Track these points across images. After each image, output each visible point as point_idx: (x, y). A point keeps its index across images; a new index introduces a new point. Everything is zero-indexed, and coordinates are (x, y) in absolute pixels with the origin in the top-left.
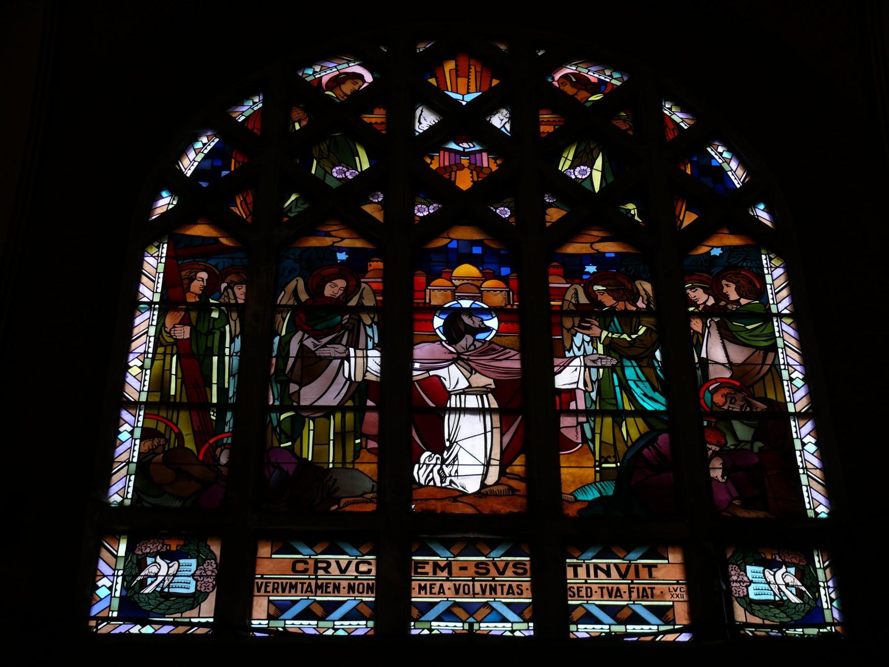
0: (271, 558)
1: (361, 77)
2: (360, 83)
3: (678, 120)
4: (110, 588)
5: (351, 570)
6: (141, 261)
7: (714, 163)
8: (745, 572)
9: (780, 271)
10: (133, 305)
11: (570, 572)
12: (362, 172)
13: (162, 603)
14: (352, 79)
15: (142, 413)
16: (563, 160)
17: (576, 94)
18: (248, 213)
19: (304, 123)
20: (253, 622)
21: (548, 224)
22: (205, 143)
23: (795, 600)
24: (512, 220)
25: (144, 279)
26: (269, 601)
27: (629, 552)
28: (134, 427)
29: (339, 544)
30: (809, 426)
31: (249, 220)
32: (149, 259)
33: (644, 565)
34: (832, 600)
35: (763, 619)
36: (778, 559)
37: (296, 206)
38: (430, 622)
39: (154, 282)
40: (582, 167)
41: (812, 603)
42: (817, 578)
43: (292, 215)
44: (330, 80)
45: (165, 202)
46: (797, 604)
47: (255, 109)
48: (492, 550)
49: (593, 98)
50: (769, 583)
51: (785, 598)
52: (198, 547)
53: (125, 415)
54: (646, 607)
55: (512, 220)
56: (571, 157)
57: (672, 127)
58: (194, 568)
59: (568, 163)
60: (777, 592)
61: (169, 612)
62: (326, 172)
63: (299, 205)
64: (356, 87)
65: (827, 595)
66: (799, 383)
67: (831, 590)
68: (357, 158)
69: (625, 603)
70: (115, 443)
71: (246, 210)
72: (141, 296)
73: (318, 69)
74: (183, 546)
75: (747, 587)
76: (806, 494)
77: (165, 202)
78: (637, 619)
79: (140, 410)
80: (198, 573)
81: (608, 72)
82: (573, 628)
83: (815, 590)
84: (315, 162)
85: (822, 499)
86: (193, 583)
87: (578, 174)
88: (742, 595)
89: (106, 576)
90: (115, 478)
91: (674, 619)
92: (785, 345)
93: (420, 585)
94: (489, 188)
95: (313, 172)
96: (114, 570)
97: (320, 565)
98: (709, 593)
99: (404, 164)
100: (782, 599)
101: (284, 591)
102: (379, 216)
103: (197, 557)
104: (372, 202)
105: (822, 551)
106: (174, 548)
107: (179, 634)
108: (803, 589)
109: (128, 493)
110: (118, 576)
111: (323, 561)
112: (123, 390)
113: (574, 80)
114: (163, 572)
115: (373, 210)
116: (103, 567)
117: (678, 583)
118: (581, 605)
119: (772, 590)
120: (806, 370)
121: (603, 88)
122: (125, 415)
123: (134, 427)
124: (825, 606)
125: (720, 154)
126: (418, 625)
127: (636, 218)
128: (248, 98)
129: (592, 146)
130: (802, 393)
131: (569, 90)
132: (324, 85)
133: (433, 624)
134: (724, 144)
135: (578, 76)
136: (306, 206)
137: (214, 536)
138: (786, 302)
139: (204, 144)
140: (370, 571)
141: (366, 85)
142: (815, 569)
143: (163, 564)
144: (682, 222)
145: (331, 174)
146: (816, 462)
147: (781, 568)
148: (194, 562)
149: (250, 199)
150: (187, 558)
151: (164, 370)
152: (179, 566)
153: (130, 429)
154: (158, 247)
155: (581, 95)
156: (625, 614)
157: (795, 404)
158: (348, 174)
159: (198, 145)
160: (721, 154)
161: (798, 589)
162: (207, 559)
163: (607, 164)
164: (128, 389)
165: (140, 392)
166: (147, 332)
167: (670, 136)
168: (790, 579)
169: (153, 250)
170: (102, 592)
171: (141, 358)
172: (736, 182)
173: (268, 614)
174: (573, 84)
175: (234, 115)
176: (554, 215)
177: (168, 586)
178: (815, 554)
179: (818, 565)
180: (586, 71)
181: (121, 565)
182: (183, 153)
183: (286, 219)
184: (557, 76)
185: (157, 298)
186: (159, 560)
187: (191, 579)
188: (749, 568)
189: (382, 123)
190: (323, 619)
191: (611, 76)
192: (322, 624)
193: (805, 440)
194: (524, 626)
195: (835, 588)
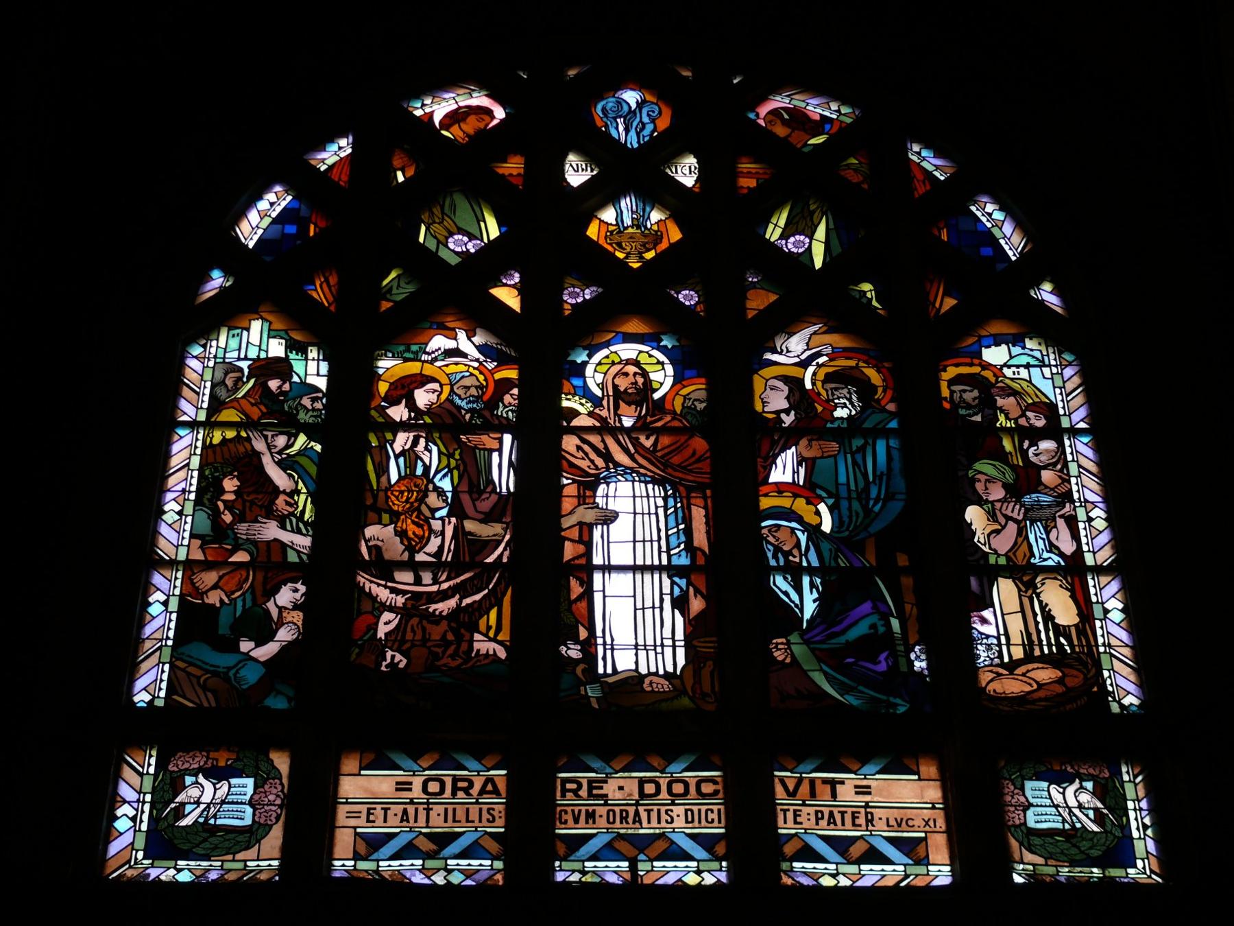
1: (489, 113)
2: (487, 118)
3: (930, 168)
4: (133, 819)
6: (182, 365)
7: (979, 228)
8: (1022, 789)
10: (169, 423)
12: (491, 243)
13: (205, 840)
14: (475, 114)
15: (180, 574)
16: (771, 227)
17: (789, 135)
18: (331, 299)
19: (410, 173)
21: (750, 314)
22: (274, 201)
23: (1095, 828)
25: (186, 392)
26: (356, 834)
27: (863, 764)
28: (168, 596)
30: (1114, 586)
31: (332, 308)
32: (194, 363)
33: (825, 781)
34: (1145, 827)
35: (1046, 859)
36: (1069, 769)
37: (399, 286)
38: (583, 861)
39: (198, 394)
40: (797, 237)
41: (1118, 833)
44: (446, 116)
45: (217, 280)
47: (343, 155)
48: (669, 764)
50: (1056, 807)
51: (1078, 825)
56: (782, 223)
57: (920, 176)
58: (250, 790)
59: (778, 232)
63: (402, 284)
64: (482, 125)
65: (1138, 817)
66: (1100, 524)
67: (1144, 813)
68: (482, 224)
69: (859, 834)
72: (180, 413)
75: (1024, 811)
77: (217, 280)
78: (873, 856)
79: (177, 570)
80: (257, 797)
81: (834, 106)
82: (785, 866)
83: (1121, 813)
84: (423, 228)
86: (249, 810)
87: (793, 245)
88: (1017, 822)
89: (129, 803)
90: (144, 666)
91: (927, 856)
93: (587, 811)
94: (674, 265)
95: (421, 240)
96: (139, 793)
98: (978, 823)
99: (547, 233)
101: (576, 821)
103: (255, 776)
105: (1131, 762)
106: (222, 764)
108: (1105, 811)
110: (144, 802)
111: (463, 779)
112: (154, 543)
113: (786, 116)
114: (206, 798)
116: (125, 791)
117: (933, 808)
118: (861, 837)
119: (1060, 815)
120: (1108, 507)
121: (827, 127)
122: (157, 579)
123: (168, 596)
124: (1135, 834)
125: (989, 212)
126: (565, 865)
127: (875, 303)
128: (332, 141)
129: (812, 207)
130: (1104, 538)
131: (781, 131)
133: (587, 864)
134: (996, 200)
138: (1082, 413)
139: (272, 204)
140: (716, 792)
141: (495, 122)
142: (1122, 783)
146: (1124, 635)
147: (1072, 782)
148: (250, 782)
149: (333, 280)
151: (1029, 635)
152: (230, 787)
153: (163, 598)
154: (204, 346)
156: (857, 850)
157: (1094, 553)
159: (263, 205)
160: (990, 215)
161: (1096, 810)
162: (268, 779)
164: (162, 543)
165: (177, 547)
166: (188, 465)
167: (921, 189)
168: (1085, 798)
170: (122, 824)
171: (181, 500)
172: (1010, 253)
173: (355, 851)
174: (785, 123)
175: (313, 162)
176: (758, 301)
177: (215, 816)
179: (1126, 778)
182: (242, 214)
184: (764, 110)
185: (202, 417)
186: (201, 779)
187: (1032, 800)
188: (1029, 785)
189: (519, 175)
190: (365, 859)
191: (838, 111)
192: (430, 864)
193: (1108, 606)
194: (715, 865)
195: (1151, 811)
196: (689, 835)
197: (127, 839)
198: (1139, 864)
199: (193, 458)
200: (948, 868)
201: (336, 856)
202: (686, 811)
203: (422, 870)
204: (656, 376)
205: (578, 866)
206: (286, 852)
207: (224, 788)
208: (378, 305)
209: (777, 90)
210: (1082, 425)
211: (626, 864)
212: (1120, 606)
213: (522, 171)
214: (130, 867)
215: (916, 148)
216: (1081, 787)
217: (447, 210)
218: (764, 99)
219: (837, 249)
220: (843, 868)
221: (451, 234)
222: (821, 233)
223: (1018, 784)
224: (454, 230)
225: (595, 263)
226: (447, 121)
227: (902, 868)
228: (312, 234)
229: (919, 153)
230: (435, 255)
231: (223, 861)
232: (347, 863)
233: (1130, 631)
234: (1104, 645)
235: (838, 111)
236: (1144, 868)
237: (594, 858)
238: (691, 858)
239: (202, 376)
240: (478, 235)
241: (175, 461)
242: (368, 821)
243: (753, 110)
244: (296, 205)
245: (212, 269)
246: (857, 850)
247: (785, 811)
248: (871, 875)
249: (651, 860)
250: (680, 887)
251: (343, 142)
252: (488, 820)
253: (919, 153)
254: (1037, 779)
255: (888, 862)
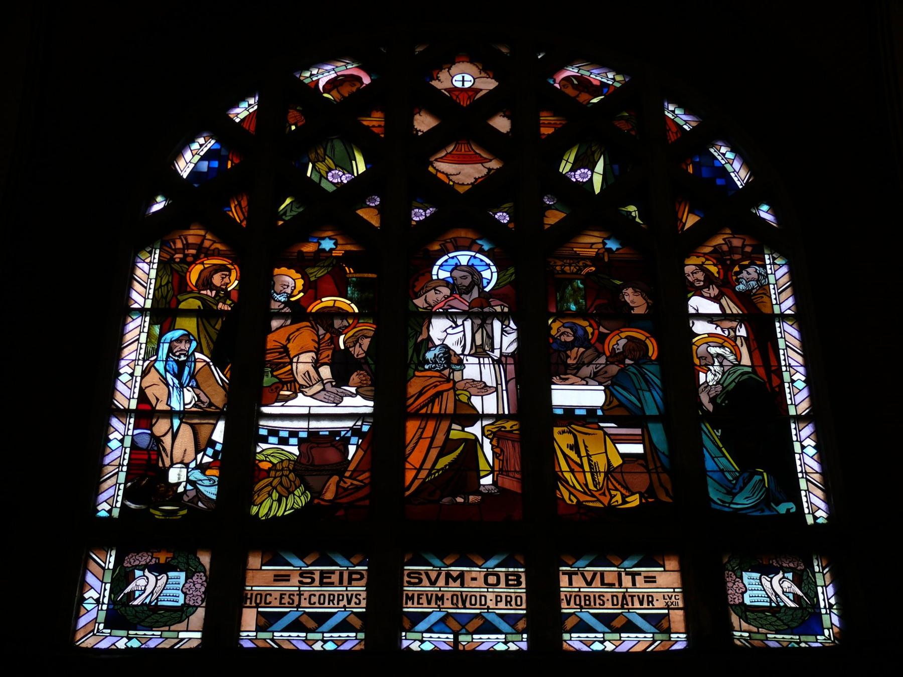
0: (261, 569)
1: (359, 79)
2: (358, 85)
3: (681, 123)
5: (662, 586)
6: (134, 266)
8: (741, 578)
9: (784, 269)
10: (126, 311)
11: (564, 580)
13: (149, 616)
15: (132, 420)
16: (564, 162)
17: (578, 96)
18: (242, 218)
20: (242, 634)
23: (793, 605)
24: (511, 226)
25: (137, 286)
28: (124, 436)
29: (330, 555)
30: (807, 430)
31: (244, 224)
35: (758, 628)
37: (291, 210)
38: (422, 633)
39: (146, 288)
40: (583, 170)
42: (815, 582)
43: (287, 218)
44: (328, 83)
45: (159, 204)
46: (791, 608)
47: (251, 110)
49: (595, 100)
51: (782, 604)
52: (188, 559)
53: (115, 422)
54: (594, 615)
55: (511, 226)
56: (572, 159)
57: (674, 129)
58: (182, 581)
59: (569, 166)
60: (773, 598)
61: (157, 625)
62: (321, 176)
66: (800, 385)
68: (354, 162)
70: (104, 450)
71: (240, 214)
73: (315, 71)
74: (173, 558)
75: (743, 593)
76: (804, 499)
77: (159, 204)
79: (130, 418)
81: (610, 75)
82: (566, 636)
84: (310, 165)
85: (822, 505)
86: (182, 596)
87: (580, 176)
88: (737, 602)
91: (669, 628)
92: (787, 346)
93: (437, 595)
94: (486, 192)
95: (309, 174)
97: (354, 576)
98: (707, 601)
99: (401, 169)
100: (778, 605)
102: (375, 222)
104: (369, 206)
105: (820, 556)
107: (165, 649)
109: (117, 501)
112: (112, 397)
113: (576, 82)
115: (370, 215)
121: (605, 90)
122: (115, 422)
125: (723, 153)
126: (411, 635)
127: (638, 220)
128: (244, 100)
129: (593, 149)
131: (570, 91)
132: (321, 87)
133: (425, 635)
135: (580, 78)
136: (301, 210)
137: (205, 548)
138: (790, 302)
139: (201, 146)
142: (814, 573)
143: (152, 578)
144: (684, 224)
145: (327, 179)
146: (816, 466)
147: (777, 573)
148: (183, 575)
149: (244, 203)
150: (176, 571)
152: (168, 578)
153: (120, 437)
155: (583, 98)
156: (617, 623)
157: (796, 406)
158: (343, 178)
159: (195, 146)
160: (724, 155)
161: (795, 595)
162: (196, 572)
163: (608, 166)
164: (118, 396)
165: (129, 400)
166: (138, 340)
167: (672, 137)
169: (144, 255)
171: (132, 365)
172: (739, 183)
175: (231, 116)
176: (553, 218)
177: (157, 598)
178: (814, 557)
179: (817, 569)
180: (588, 74)
181: (108, 578)
182: (179, 153)
183: (280, 223)
185: (148, 305)
186: (147, 573)
188: (745, 575)
189: (380, 126)
190: (313, 631)
192: (311, 636)
193: (805, 444)
194: (518, 637)
196: (641, 615)
197: (93, 615)
198: (826, 632)
199: (142, 334)
200: (684, 636)
201: (242, 629)
202: (612, 596)
203: (306, 641)
204: (486, 274)
205: (418, 636)
206: (207, 629)
207: (163, 578)
208: (277, 223)
209: (570, 63)
210: (789, 312)
211: (451, 636)
212: (813, 444)
213: (383, 124)
214: (94, 635)
215: (671, 108)
216: (784, 577)
217: (328, 153)
218: (561, 67)
219: (611, 181)
220: (608, 636)
221: (330, 170)
222: (600, 167)
223: (739, 574)
224: (333, 166)
225: (439, 192)
226: (328, 87)
227: (651, 635)
228: (229, 166)
229: (673, 112)
230: (318, 185)
231: (162, 631)
232: (251, 634)
233: (821, 462)
234: (801, 472)
235: (614, 79)
236: (829, 635)
237: (430, 630)
238: (500, 632)
239: (148, 275)
240: (349, 169)
241: (129, 337)
242: (281, 603)
243: (552, 77)
244: (217, 146)
245: (157, 195)
246: (617, 623)
247: (632, 597)
248: (630, 642)
249: (472, 634)
250: (492, 653)
251: (252, 101)
252: (356, 603)
253: (673, 112)
254: (752, 571)
255: (641, 631)
